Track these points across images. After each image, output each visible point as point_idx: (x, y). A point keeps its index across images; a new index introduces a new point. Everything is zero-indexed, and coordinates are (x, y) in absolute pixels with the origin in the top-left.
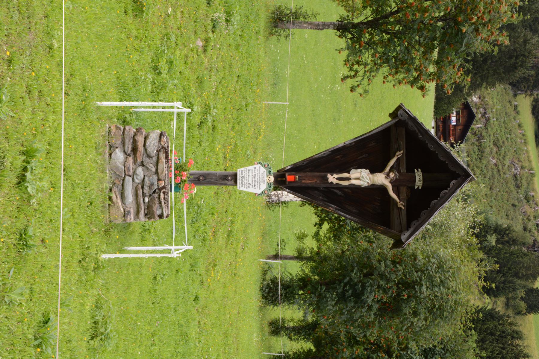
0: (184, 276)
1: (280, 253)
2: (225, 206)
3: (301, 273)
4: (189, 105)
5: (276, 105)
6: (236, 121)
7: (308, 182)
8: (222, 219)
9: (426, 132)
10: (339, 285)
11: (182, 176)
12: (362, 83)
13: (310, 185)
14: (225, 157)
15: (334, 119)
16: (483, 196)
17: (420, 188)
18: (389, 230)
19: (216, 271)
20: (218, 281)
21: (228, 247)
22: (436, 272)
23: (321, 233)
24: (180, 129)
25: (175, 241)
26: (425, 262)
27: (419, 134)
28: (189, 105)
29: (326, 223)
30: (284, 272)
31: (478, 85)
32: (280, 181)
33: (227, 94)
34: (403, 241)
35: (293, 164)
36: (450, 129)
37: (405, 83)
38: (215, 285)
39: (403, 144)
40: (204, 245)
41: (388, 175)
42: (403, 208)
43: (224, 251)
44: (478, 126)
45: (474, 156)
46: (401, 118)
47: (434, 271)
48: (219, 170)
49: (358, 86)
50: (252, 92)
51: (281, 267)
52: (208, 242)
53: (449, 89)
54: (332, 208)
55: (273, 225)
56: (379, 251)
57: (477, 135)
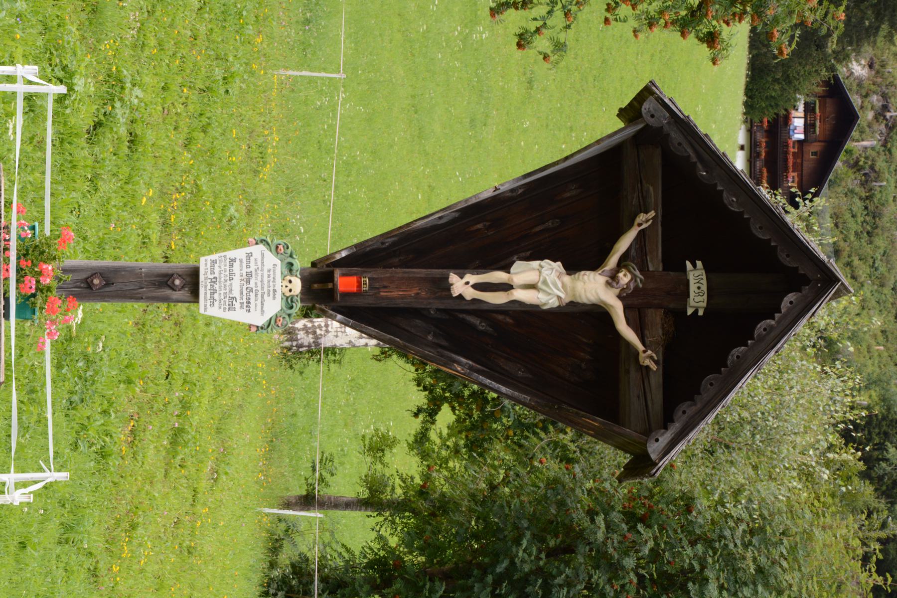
0: (43, 558)
1: (320, 491)
2: (165, 359)
3: (376, 546)
4: (61, 74)
5: (311, 80)
6: (196, 123)
7: (395, 294)
8: (156, 395)
9: (719, 162)
10: (481, 580)
11: (40, 273)
12: (548, 22)
13: (401, 304)
14: (165, 224)
15: (472, 120)
16: (875, 336)
17: (701, 313)
18: (616, 428)
19: (135, 542)
20: (142, 571)
21: (173, 473)
22: (746, 546)
23: (433, 435)
24: (34, 141)
25: (17, 459)
26: (716, 515)
27: (699, 166)
28: (61, 74)
29: (446, 408)
30: (329, 544)
31: (867, 30)
32: (320, 290)
33: (170, 45)
34: (653, 457)
35: (356, 246)
36: (787, 153)
37: (666, 26)
38: (131, 582)
39: (654, 192)
40: (102, 471)
41: (613, 278)
42: (654, 367)
43: (159, 486)
44: (865, 143)
45: (853, 226)
46: (651, 121)
47: (739, 542)
48: (149, 260)
49: (538, 30)
50: (243, 43)
51: (322, 530)
52: (114, 462)
53: (784, 44)
54: (461, 365)
55: (301, 412)
56: (589, 484)
57: (862, 168)
